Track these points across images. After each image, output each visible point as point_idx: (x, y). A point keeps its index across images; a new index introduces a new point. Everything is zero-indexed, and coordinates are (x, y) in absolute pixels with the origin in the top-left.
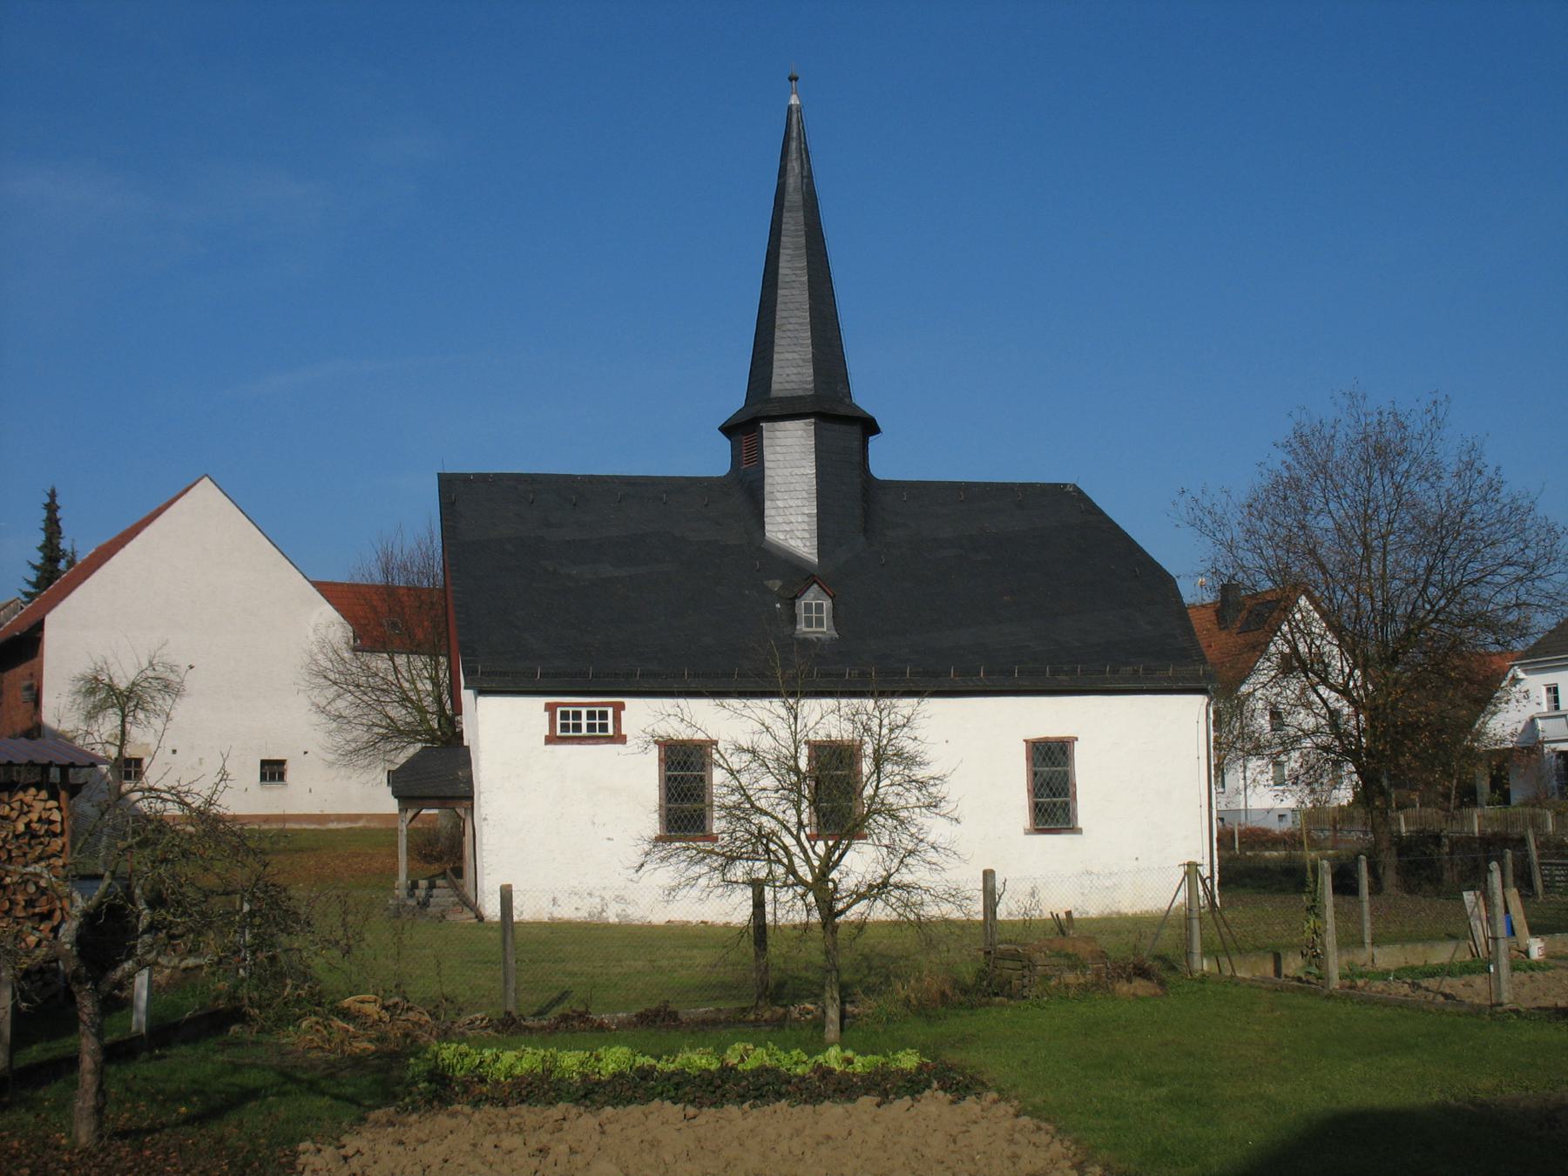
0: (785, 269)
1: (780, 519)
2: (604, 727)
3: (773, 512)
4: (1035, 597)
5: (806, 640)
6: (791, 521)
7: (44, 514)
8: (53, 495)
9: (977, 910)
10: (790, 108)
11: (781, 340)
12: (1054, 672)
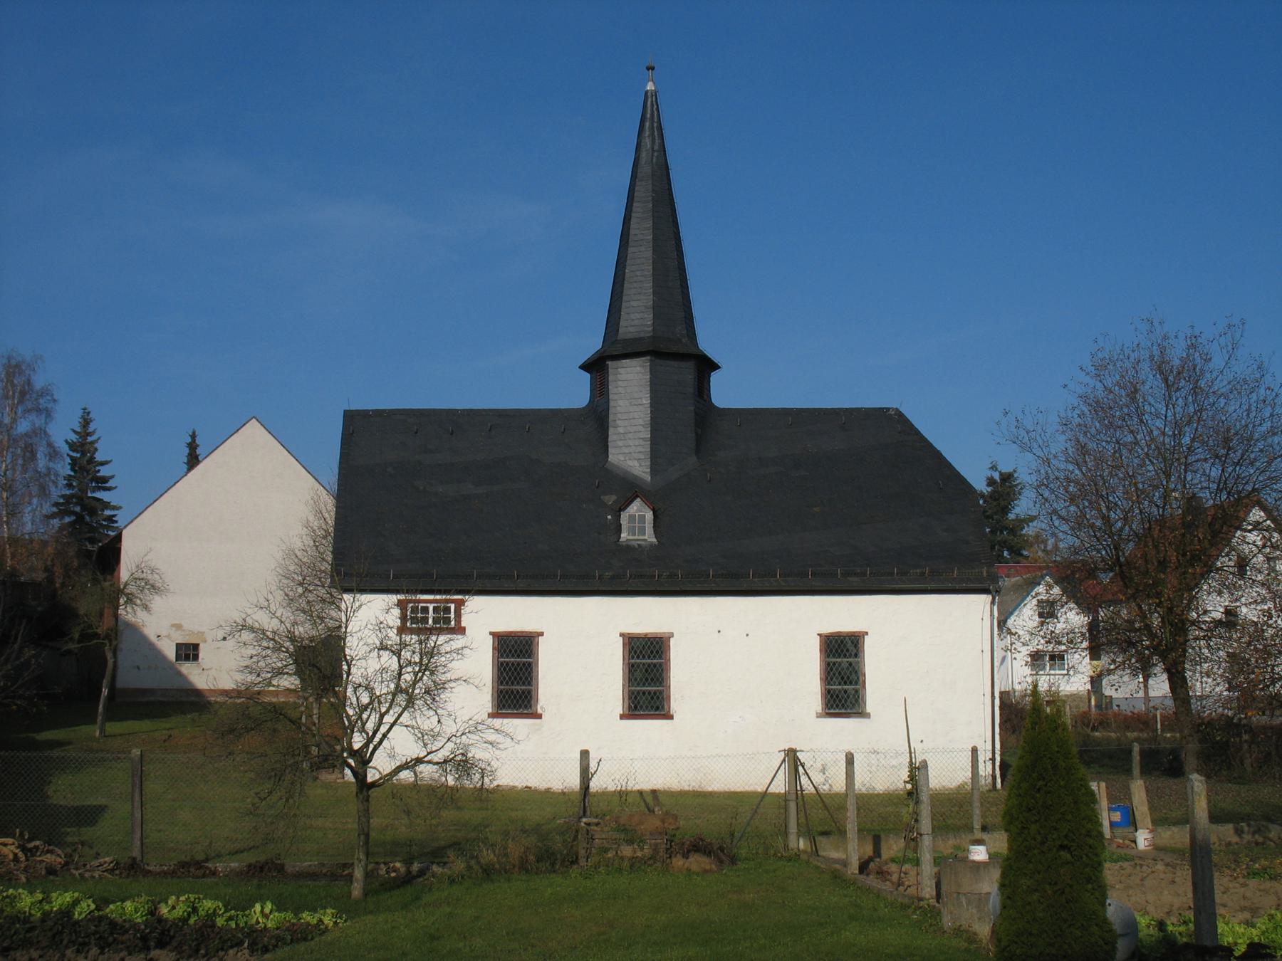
0: (634, 230)
1: (620, 443)
2: (447, 620)
3: (615, 437)
4: (845, 508)
5: (628, 546)
6: (630, 448)
7: (187, 451)
8: (193, 436)
9: (574, 782)
10: (647, 92)
11: (629, 289)
12: (845, 575)
